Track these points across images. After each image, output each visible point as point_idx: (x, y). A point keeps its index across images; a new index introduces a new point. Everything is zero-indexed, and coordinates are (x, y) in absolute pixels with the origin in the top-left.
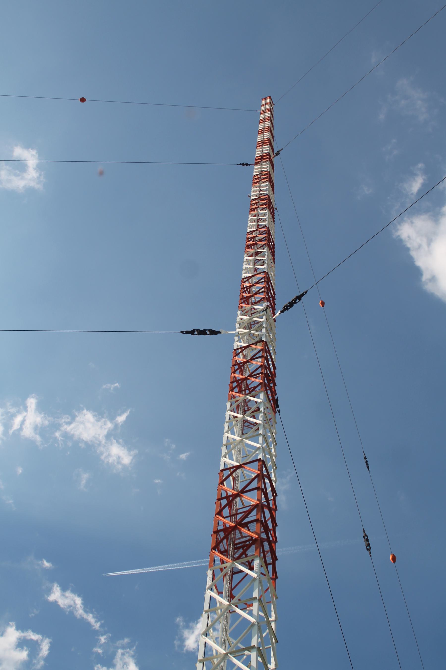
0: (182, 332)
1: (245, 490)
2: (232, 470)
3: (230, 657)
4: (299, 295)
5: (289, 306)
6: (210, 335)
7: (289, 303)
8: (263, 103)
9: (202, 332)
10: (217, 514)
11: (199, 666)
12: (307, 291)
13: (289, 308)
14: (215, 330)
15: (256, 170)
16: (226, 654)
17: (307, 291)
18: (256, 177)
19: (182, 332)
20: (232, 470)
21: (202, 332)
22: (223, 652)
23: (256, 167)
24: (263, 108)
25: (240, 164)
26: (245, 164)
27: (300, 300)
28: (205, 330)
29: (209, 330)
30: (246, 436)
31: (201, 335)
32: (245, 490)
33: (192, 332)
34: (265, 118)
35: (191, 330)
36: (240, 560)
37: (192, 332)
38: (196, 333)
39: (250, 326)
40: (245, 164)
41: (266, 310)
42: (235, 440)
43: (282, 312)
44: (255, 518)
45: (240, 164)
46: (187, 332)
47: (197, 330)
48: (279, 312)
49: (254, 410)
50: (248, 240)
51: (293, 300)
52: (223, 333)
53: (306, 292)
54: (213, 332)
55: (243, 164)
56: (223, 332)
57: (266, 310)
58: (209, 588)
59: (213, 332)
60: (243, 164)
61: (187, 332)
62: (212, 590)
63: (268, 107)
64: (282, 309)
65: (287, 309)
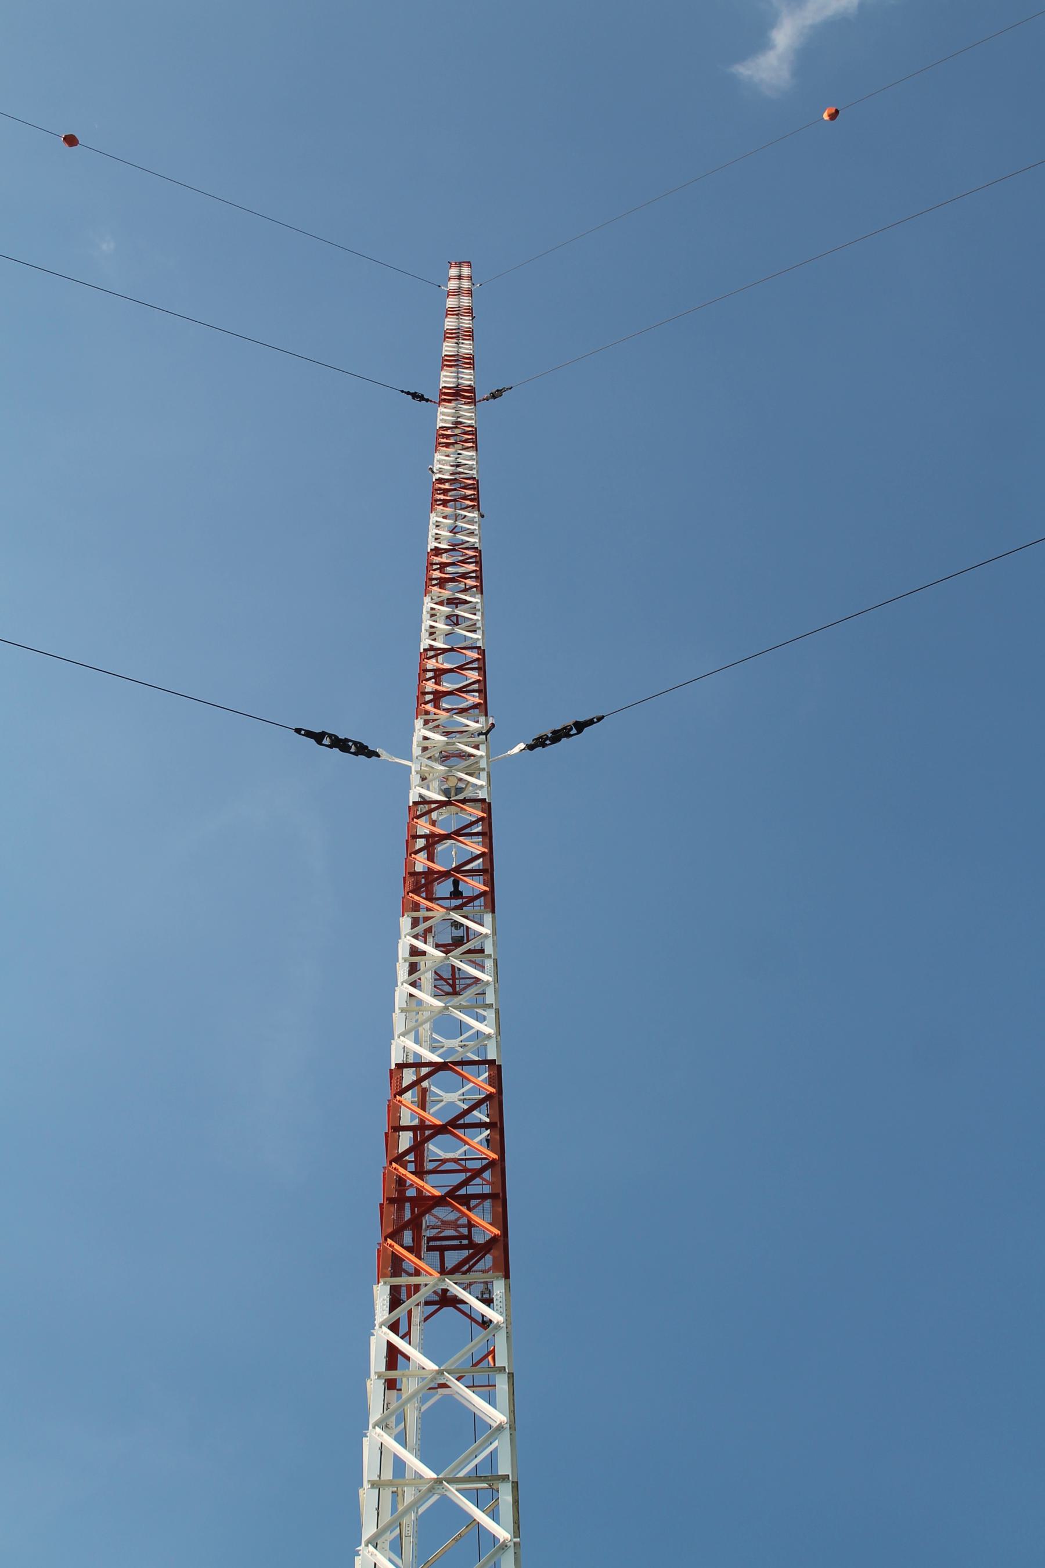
0: (298, 731)
1: (461, 1122)
2: (433, 806)
3: (448, 1490)
4: (581, 719)
5: (547, 738)
6: (355, 754)
7: (554, 732)
8: (453, 272)
9: (340, 744)
10: (391, 1236)
11: (367, 1555)
12: (603, 717)
13: (548, 742)
14: (367, 747)
15: (444, 415)
16: (439, 1481)
17: (603, 717)
18: (445, 440)
19: (298, 731)
20: (433, 806)
21: (340, 744)
22: (429, 1474)
23: (441, 409)
24: (453, 285)
25: (408, 393)
26: (418, 397)
27: (579, 731)
28: (347, 740)
29: (355, 743)
30: (456, 1000)
31: (336, 750)
32: (461, 1122)
33: (318, 737)
34: (460, 288)
35: (317, 730)
36: (458, 1276)
37: (318, 737)
38: (327, 741)
39: (445, 757)
40: (418, 397)
41: (486, 734)
42: (421, 1477)
43: (530, 747)
44: (487, 1189)
45: (408, 393)
46: (309, 734)
47: (330, 736)
48: (522, 746)
49: (472, 947)
50: (436, 490)
51: (565, 728)
52: (383, 757)
53: (600, 719)
54: (363, 750)
55: (415, 396)
56: (385, 755)
57: (486, 734)
58: (377, 1424)
59: (363, 750)
60: (415, 396)
61: (309, 734)
62: (386, 1427)
63: (466, 284)
64: (531, 742)
65: (544, 745)
